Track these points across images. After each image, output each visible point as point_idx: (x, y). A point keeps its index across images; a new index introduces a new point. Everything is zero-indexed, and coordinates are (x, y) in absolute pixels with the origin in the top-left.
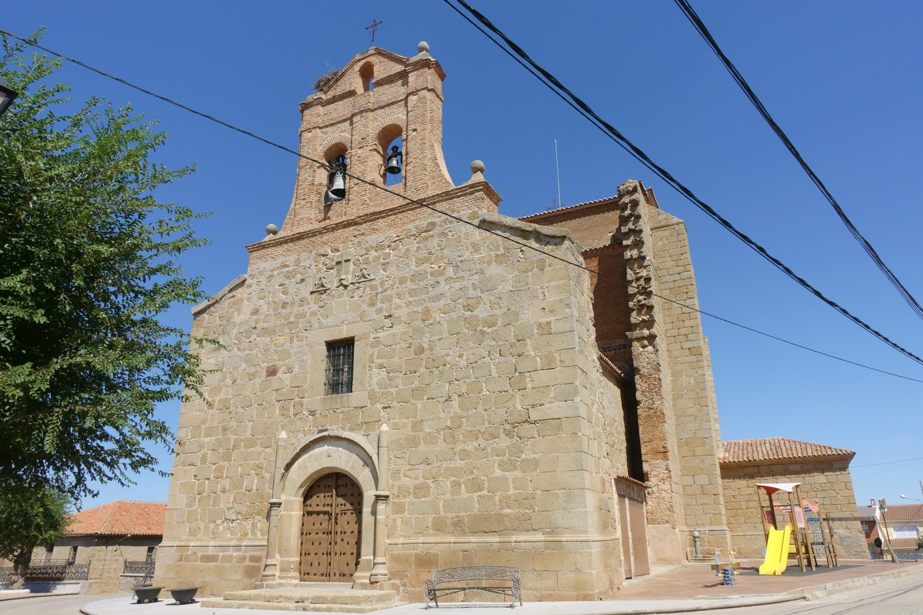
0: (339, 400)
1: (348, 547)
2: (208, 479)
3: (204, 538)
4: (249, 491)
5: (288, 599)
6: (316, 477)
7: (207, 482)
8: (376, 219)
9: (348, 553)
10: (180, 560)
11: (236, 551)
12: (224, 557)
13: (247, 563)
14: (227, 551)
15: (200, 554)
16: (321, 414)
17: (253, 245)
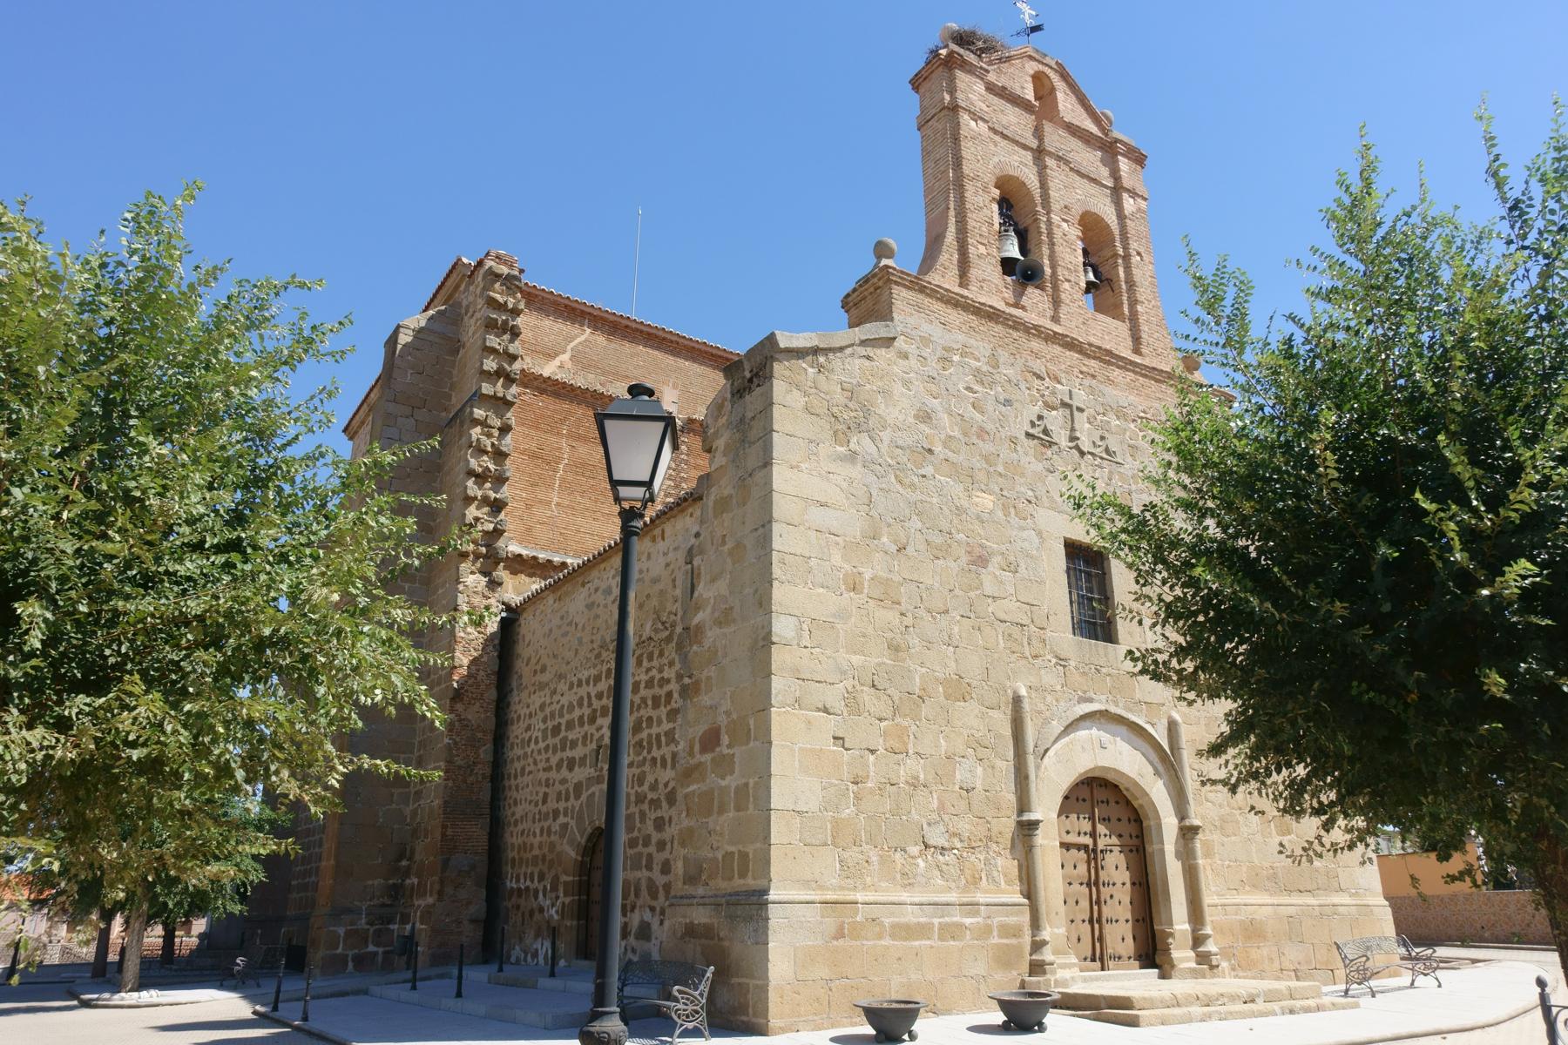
0: (1102, 652)
1: (1120, 908)
2: (872, 752)
3: (884, 884)
4: (968, 791)
5: (1234, 998)
6: (1110, 777)
7: (872, 758)
8: (1109, 363)
9: (1122, 920)
10: (840, 934)
11: (969, 915)
12: (942, 927)
13: (995, 940)
14: (949, 915)
15: (887, 921)
16: (1077, 668)
17: (902, 272)
